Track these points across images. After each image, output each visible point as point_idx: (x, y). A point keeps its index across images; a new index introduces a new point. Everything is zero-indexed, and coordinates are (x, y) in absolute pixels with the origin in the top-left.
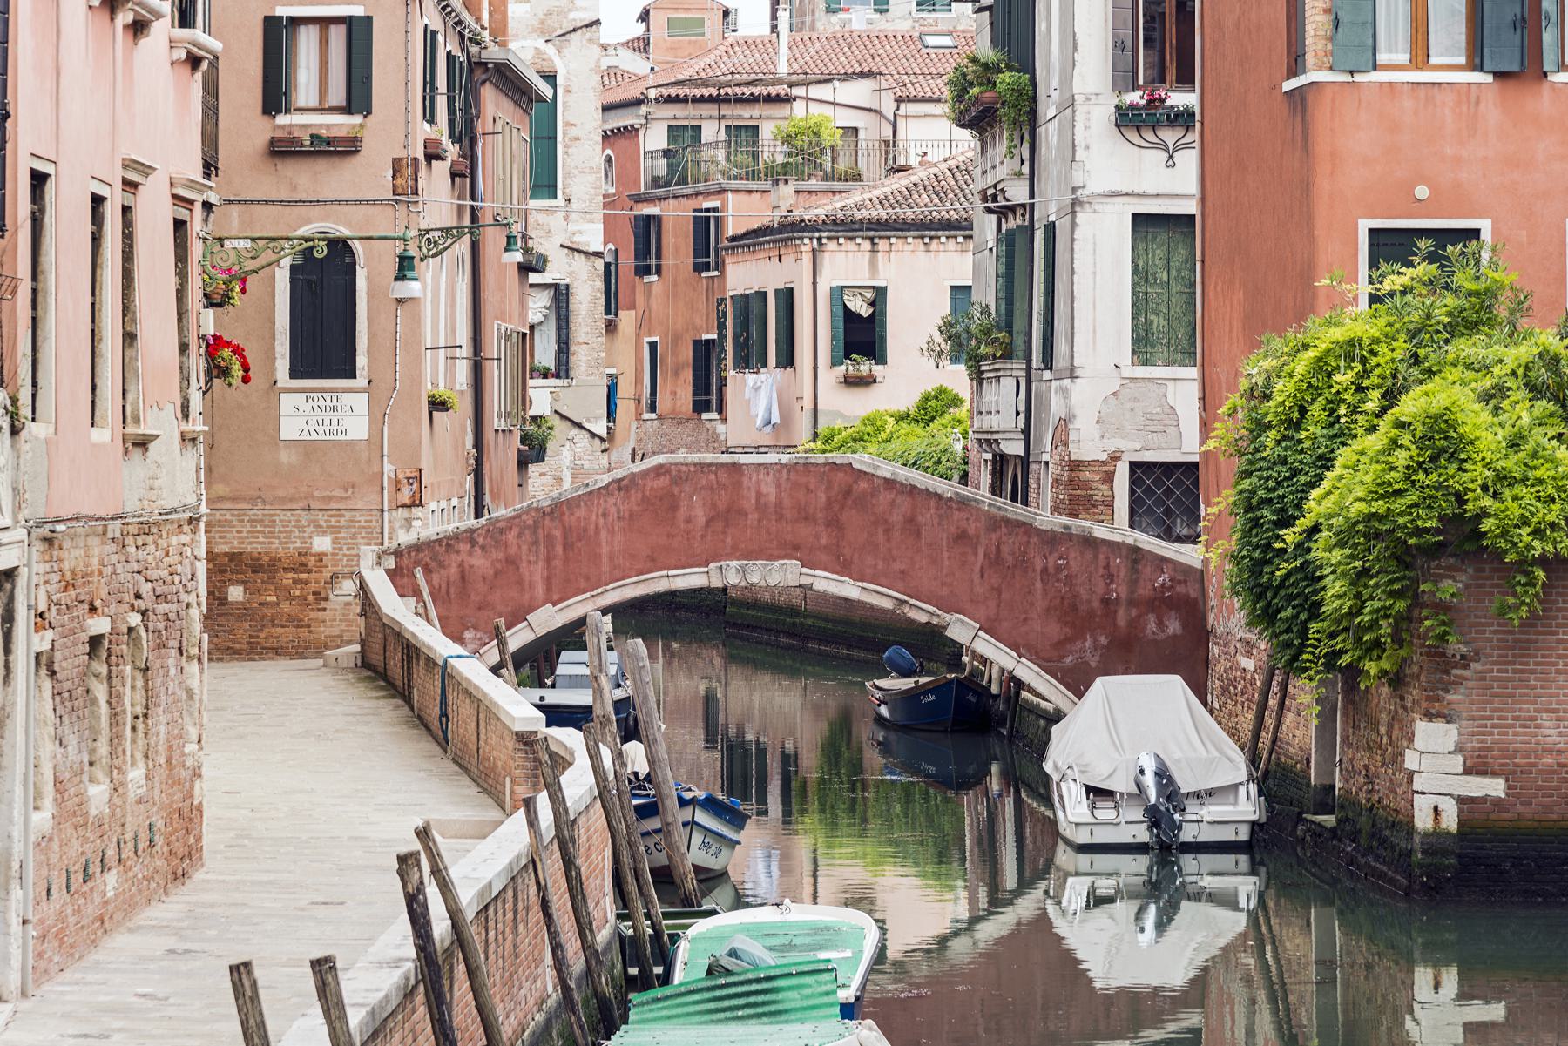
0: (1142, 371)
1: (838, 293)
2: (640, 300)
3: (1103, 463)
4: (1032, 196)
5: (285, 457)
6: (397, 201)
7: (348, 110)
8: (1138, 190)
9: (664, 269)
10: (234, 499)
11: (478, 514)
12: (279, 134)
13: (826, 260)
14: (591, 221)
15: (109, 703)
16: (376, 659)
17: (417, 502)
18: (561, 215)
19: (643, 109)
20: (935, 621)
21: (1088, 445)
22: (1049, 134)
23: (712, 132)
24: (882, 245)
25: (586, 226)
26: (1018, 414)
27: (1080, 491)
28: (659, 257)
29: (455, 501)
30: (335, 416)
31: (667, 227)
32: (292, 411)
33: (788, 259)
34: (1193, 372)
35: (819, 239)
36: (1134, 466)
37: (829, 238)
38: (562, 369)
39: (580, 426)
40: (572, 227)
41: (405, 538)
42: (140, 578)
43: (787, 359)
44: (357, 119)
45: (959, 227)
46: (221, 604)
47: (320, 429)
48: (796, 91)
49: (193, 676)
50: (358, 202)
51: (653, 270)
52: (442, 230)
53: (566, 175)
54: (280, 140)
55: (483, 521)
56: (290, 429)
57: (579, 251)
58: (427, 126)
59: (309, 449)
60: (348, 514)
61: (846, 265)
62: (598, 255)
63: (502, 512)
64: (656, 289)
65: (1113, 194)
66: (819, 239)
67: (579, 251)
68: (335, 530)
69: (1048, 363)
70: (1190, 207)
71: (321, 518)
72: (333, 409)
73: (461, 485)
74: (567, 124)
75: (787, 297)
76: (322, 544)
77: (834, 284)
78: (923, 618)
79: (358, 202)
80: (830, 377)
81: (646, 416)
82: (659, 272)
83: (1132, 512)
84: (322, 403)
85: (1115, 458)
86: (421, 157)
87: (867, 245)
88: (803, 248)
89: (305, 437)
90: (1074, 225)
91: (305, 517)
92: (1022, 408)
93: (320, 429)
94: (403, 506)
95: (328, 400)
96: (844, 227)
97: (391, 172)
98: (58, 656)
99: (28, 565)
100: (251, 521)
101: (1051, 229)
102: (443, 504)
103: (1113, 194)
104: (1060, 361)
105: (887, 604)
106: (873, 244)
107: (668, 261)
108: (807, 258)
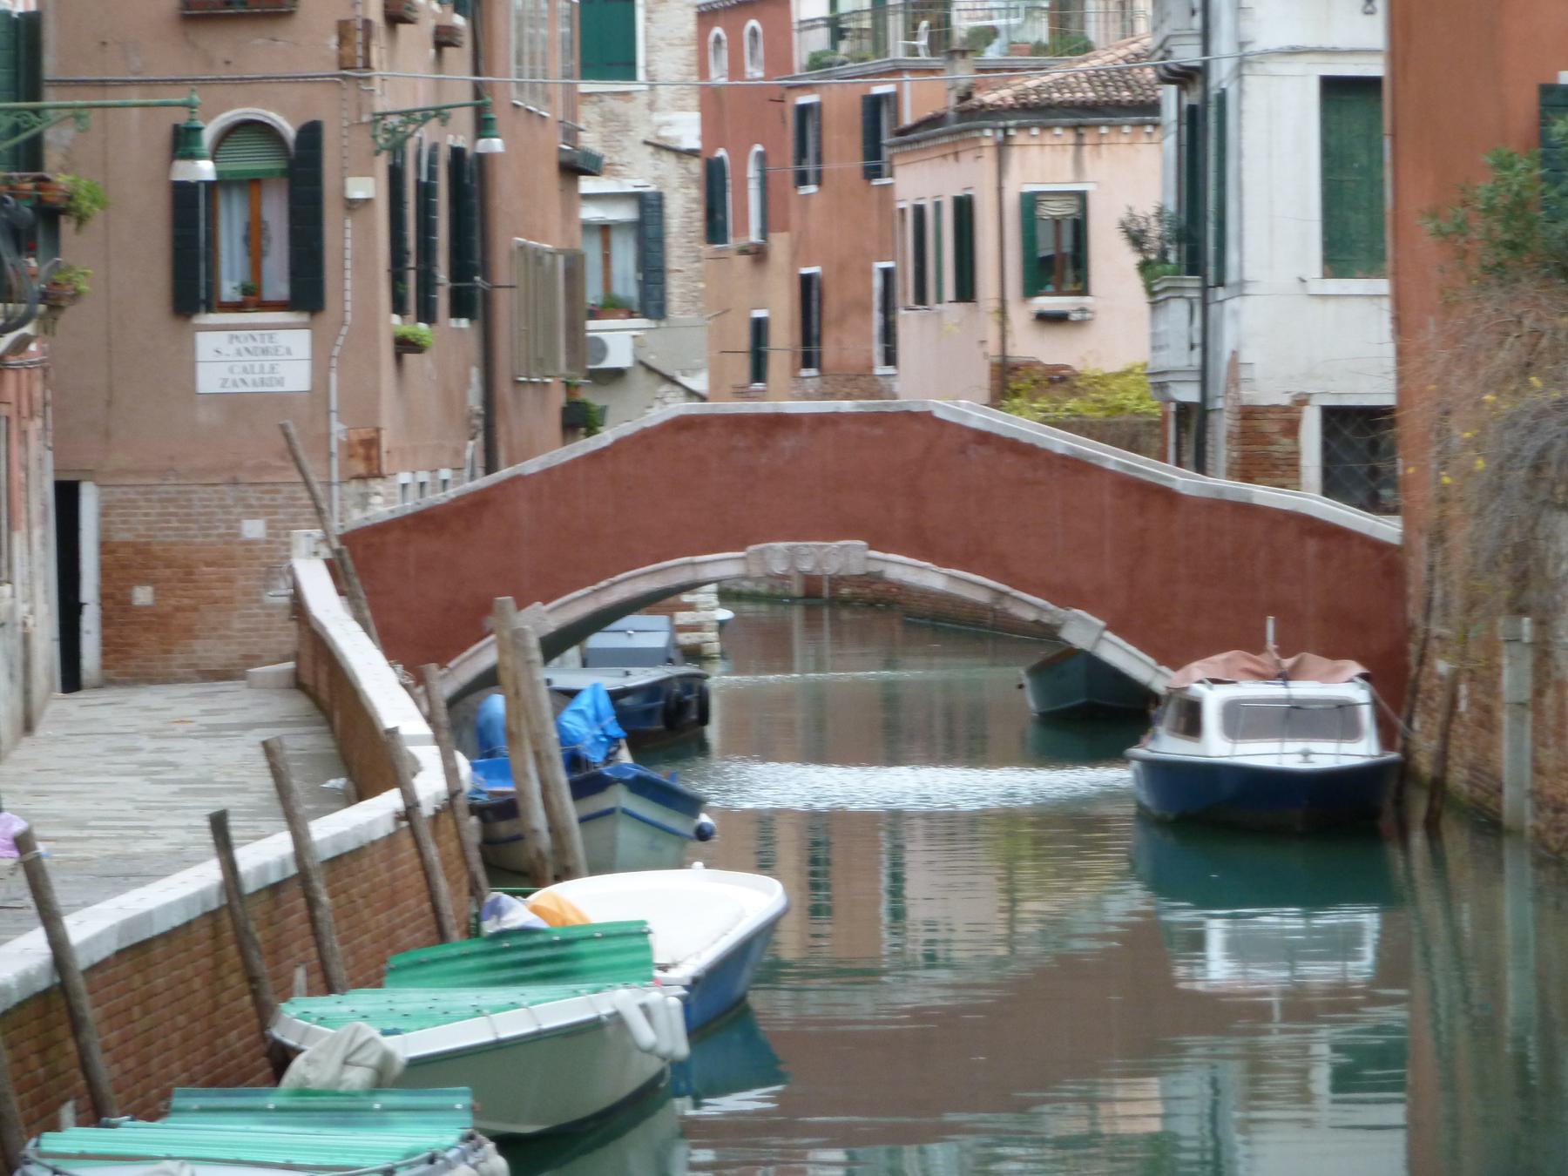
0: (1335, 286)
1: (1030, 202)
2: (794, 217)
3: (1286, 409)
4: (1206, 50)
5: (204, 415)
6: (344, 77)
8: (1327, 44)
9: (825, 175)
10: (140, 472)
13: (1015, 156)
14: (683, 109)
16: (307, 679)
20: (1046, 619)
21: (1267, 390)
25: (677, 116)
26: (1192, 347)
27: (1262, 442)
28: (819, 159)
31: (830, 115)
33: (967, 158)
34: (1383, 286)
35: (1005, 129)
37: (1019, 128)
39: (671, 380)
40: (657, 118)
41: (357, 518)
43: (966, 290)
45: (1147, 110)
46: (125, 610)
50: (294, 79)
51: (811, 177)
52: (401, 113)
53: (650, 49)
56: (210, 379)
59: (236, 405)
60: (286, 489)
61: (1042, 164)
62: (692, 153)
66: (1005, 129)
68: (267, 511)
69: (1221, 283)
70: (1374, 68)
71: (252, 495)
72: (265, 351)
73: (458, 453)
75: (964, 209)
76: (254, 529)
77: (1028, 188)
78: (1030, 615)
79: (294, 79)
80: (1021, 315)
82: (819, 182)
83: (1327, 474)
84: (250, 344)
85: (1302, 401)
87: (1069, 137)
88: (985, 142)
90: (1241, 92)
91: (230, 494)
92: (1197, 339)
93: (249, 378)
95: (260, 339)
97: (333, 41)
100: (161, 501)
101: (1222, 98)
102: (423, 476)
103: (1294, 52)
104: (1232, 276)
105: (982, 597)
106: (1080, 136)
107: (831, 166)
108: (989, 156)
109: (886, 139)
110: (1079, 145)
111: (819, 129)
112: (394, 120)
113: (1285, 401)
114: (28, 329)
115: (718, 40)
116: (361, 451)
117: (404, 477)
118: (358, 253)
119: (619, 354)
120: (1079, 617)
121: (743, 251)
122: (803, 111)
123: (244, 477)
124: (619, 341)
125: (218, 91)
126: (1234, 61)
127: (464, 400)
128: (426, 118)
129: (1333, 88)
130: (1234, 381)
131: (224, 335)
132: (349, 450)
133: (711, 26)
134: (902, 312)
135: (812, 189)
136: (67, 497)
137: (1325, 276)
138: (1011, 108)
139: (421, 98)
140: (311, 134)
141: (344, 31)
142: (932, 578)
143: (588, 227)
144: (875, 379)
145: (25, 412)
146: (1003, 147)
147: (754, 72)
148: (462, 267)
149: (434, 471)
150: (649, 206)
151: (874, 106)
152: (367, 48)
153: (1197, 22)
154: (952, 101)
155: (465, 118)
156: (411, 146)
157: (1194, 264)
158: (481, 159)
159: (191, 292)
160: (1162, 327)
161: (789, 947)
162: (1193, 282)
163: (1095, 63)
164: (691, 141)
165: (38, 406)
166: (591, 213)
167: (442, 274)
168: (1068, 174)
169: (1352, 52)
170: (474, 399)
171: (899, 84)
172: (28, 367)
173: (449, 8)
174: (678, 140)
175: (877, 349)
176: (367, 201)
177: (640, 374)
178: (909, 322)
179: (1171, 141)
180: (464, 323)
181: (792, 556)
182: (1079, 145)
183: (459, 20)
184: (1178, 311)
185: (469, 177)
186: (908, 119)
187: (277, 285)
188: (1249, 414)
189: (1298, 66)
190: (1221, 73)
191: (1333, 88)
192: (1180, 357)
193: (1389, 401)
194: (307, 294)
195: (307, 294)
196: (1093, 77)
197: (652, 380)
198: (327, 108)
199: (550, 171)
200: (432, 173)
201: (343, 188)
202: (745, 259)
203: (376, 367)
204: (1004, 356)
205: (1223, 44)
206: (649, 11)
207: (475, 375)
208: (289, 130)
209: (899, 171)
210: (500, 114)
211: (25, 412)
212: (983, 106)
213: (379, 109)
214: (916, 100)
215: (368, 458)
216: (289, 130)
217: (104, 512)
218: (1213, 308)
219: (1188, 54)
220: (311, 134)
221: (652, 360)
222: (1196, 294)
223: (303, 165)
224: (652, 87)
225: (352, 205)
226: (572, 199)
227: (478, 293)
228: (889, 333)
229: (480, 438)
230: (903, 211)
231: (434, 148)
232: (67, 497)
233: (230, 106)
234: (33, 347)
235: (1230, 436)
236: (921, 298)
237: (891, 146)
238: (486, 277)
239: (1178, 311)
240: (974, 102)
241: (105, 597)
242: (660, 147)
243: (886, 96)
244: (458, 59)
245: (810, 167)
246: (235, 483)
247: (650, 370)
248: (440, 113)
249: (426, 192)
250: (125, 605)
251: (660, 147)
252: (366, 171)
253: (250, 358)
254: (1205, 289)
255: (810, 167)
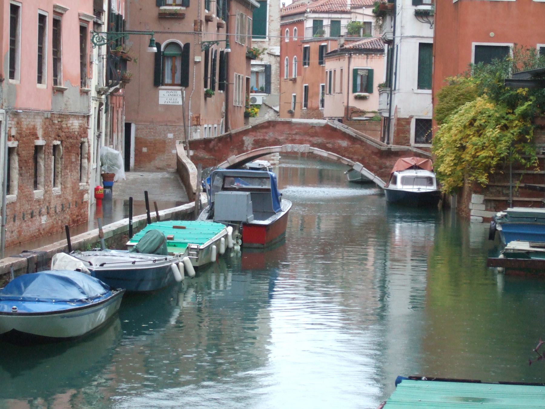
1: (355, 71)
3: (408, 119)
4: (394, 35)
6: (195, 33)
7: (182, 5)
8: (421, 35)
10: (145, 122)
11: (226, 131)
12: (161, 12)
13: (352, 60)
14: (276, 46)
15: (44, 166)
17: (198, 124)
18: (267, 43)
19: (306, 15)
21: (403, 114)
22: (398, 18)
23: (326, 22)
24: (370, 57)
25: (275, 47)
28: (309, 59)
29: (216, 126)
30: (175, 98)
31: (311, 50)
32: (162, 96)
33: (342, 60)
34: (430, 91)
35: (350, 54)
36: (417, 120)
37: (354, 54)
38: (267, 89)
42: (60, 131)
44: (183, 8)
45: (382, 51)
47: (171, 101)
48: (353, 10)
49: (85, 163)
53: (269, 31)
54: (162, 14)
55: (227, 133)
56: (162, 101)
57: (273, 55)
58: (207, 11)
59: (167, 107)
61: (360, 63)
62: (278, 56)
63: (233, 132)
64: (307, 70)
65: (413, 37)
67: (273, 55)
68: (174, 132)
70: (431, 41)
72: (175, 95)
73: (219, 121)
74: (270, 16)
77: (355, 68)
81: (304, 108)
82: (309, 65)
84: (171, 94)
85: (411, 117)
86: (204, 20)
87: (365, 56)
89: (166, 103)
92: (389, 102)
93: (171, 101)
94: (195, 125)
96: (359, 51)
97: (193, 24)
98: (20, 149)
99: (6, 120)
100: (150, 128)
102: (210, 126)
103: (413, 37)
107: (311, 61)
108: (347, 59)
109: (324, 55)
110: (367, 58)
111: (309, 53)
112: (206, 43)
113: (408, 117)
114: (118, 86)
115: (287, 31)
116: (196, 119)
117: (206, 126)
118: (197, 74)
119: (259, 102)
120: (358, 165)
121: (291, 80)
122: (306, 49)
123: (169, 124)
124: (260, 98)
125: (166, 35)
126: (400, 38)
127: (221, 109)
128: (213, 44)
129: (422, 45)
130: (396, 112)
131: (166, 91)
132: (193, 119)
133: (286, 28)
134: (325, 95)
135: (307, 66)
136: (128, 127)
137: (418, 88)
138: (352, 49)
139: (213, 38)
140: (187, 46)
141: (195, 23)
142: (324, 153)
143: (252, 72)
144: (319, 110)
145: (118, 106)
146: (350, 58)
147: (295, 39)
148: (221, 78)
149: (213, 125)
150: (268, 68)
151: (322, 48)
152: (201, 27)
153: (392, 29)
154: (339, 47)
155: (224, 43)
156: (210, 49)
157: (390, 86)
158: (227, 53)
159: (158, 81)
160: (381, 99)
161: (185, 145)
162: (388, 89)
163: (372, 39)
164: (278, 53)
165: (121, 105)
166: (255, 69)
167: (209, 76)
168: (366, 65)
169: (427, 37)
170: (223, 110)
171: (328, 43)
172: (120, 96)
173: (221, 19)
174: (275, 53)
175: (320, 105)
176: (199, 62)
177: (264, 106)
178: (327, 98)
179: (386, 58)
180: (222, 91)
181: (292, 148)
182: (367, 58)
183: (224, 22)
184: (385, 96)
185: (224, 58)
186: (329, 51)
187: (178, 80)
188: (399, 119)
189: (414, 40)
190: (397, 41)
191: (422, 45)
192: (385, 106)
193: (431, 118)
194: (185, 82)
195: (185, 82)
196: (371, 43)
197: (266, 108)
198: (190, 40)
199: (244, 58)
200: (215, 56)
201: (194, 59)
202: (291, 82)
203: (200, 99)
204: (348, 106)
205: (398, 33)
206: (269, 23)
207: (224, 103)
208: (182, 45)
209: (326, 63)
210: (232, 44)
211: (118, 106)
212: (346, 48)
213: (203, 41)
214: (332, 47)
215: (197, 121)
216: (182, 45)
217: (137, 130)
218: (393, 96)
219: (390, 37)
220: (187, 46)
221: (267, 103)
222: (389, 92)
223: (185, 53)
224: (270, 39)
225: (196, 63)
226: (249, 65)
227: (225, 85)
228: (323, 101)
229: (224, 118)
230: (327, 72)
231: (216, 51)
232: (128, 127)
233: (169, 39)
234: (121, 91)
235: (395, 124)
236: (330, 92)
237: (325, 57)
238: (227, 81)
239: (385, 96)
240: (344, 47)
241: (136, 150)
242: (270, 54)
243: (325, 46)
244: (223, 31)
245: (307, 61)
246: (166, 125)
247: (266, 105)
248: (217, 42)
249: (214, 61)
250: (141, 152)
251: (270, 54)
252: (199, 55)
253: (169, 96)
254: (391, 91)
255: (307, 61)
